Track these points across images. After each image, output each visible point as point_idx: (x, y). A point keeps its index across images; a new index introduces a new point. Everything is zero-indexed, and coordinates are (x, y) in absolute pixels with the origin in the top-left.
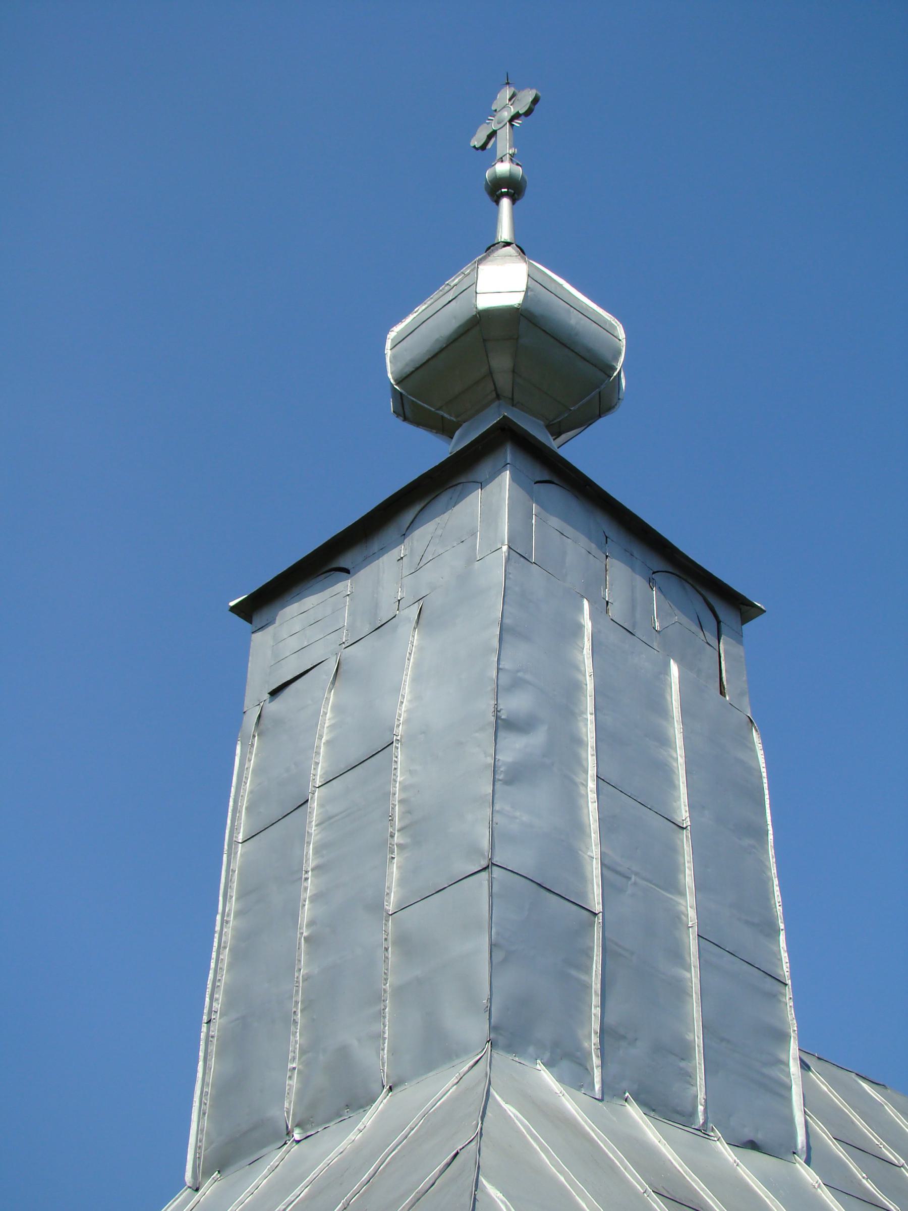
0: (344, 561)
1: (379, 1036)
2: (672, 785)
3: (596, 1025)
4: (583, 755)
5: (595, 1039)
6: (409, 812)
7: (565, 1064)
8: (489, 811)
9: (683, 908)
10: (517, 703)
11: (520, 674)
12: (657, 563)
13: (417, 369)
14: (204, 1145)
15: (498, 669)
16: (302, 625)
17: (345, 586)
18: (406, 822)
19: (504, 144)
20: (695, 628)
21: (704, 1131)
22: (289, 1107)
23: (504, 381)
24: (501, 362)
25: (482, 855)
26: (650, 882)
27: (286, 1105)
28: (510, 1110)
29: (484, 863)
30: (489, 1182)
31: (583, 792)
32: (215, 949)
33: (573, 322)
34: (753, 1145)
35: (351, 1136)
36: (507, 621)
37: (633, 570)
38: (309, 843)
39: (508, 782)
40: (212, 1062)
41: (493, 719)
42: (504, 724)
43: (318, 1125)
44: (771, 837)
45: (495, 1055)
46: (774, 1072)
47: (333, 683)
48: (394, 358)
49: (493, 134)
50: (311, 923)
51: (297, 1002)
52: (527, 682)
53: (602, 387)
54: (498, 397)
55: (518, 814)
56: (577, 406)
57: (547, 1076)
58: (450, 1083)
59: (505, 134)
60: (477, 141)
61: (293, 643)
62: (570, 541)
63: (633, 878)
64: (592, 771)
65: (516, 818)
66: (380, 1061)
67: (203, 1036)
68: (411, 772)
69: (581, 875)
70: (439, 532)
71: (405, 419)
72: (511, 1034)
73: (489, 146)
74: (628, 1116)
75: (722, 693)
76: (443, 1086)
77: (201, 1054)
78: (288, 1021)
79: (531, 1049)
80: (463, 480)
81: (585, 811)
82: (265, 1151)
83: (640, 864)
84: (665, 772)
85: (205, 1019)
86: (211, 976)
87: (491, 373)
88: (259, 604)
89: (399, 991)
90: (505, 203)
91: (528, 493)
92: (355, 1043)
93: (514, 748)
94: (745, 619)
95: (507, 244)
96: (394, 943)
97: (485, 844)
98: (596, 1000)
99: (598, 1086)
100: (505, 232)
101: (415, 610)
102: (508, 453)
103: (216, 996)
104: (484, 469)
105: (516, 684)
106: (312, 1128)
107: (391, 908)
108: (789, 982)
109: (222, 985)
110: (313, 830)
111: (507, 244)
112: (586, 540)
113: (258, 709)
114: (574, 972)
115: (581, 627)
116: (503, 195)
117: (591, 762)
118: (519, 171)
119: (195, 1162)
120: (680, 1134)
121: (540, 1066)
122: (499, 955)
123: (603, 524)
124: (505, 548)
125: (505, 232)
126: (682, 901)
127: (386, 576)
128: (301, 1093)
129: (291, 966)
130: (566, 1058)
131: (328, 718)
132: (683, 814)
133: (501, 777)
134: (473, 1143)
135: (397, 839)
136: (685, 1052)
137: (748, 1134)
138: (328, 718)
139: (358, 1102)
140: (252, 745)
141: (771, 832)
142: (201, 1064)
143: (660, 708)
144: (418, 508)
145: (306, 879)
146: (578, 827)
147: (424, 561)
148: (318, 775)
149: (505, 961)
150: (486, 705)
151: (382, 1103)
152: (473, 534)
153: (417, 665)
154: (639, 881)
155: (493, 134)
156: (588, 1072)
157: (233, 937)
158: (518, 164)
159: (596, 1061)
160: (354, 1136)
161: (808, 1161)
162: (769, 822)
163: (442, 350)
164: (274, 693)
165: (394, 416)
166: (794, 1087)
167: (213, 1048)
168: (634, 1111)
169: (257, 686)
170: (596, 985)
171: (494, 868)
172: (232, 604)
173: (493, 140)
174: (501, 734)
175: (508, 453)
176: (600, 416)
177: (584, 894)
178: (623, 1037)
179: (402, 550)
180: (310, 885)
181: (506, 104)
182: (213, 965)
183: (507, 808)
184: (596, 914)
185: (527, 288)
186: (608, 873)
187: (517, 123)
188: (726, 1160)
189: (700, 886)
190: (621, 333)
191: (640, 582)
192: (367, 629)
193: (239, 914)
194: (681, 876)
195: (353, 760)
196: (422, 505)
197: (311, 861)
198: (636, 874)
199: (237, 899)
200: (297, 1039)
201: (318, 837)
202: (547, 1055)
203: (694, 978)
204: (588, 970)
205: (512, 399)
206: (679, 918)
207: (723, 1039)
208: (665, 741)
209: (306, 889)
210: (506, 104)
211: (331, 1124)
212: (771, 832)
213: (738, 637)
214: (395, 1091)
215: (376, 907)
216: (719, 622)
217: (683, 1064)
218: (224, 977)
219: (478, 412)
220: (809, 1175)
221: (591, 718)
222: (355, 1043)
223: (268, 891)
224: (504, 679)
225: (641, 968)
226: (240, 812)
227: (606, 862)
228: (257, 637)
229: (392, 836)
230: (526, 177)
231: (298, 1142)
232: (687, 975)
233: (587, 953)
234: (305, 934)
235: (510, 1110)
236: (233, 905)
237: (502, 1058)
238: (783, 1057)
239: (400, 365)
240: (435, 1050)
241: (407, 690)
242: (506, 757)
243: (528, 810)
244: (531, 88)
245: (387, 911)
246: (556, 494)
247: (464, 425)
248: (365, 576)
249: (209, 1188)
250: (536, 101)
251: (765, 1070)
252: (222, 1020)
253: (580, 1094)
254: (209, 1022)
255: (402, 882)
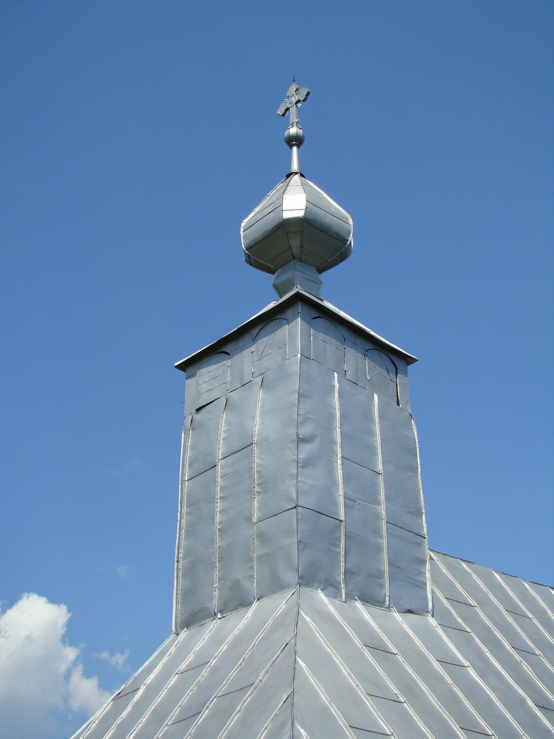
0: (227, 349)
1: (252, 576)
2: (375, 454)
3: (342, 570)
4: (336, 448)
5: (342, 576)
6: (261, 477)
7: (330, 589)
8: (295, 481)
9: (380, 511)
10: (306, 430)
11: (307, 416)
12: (368, 346)
13: (256, 244)
14: (179, 615)
15: (298, 415)
16: (210, 379)
17: (228, 362)
18: (260, 481)
19: (293, 115)
20: (386, 373)
21: (389, 607)
22: (215, 604)
23: (296, 251)
24: (295, 243)
25: (293, 501)
26: (365, 501)
27: (214, 603)
28: (308, 619)
29: (294, 505)
30: (300, 659)
31: (336, 465)
32: (178, 528)
33: (328, 221)
34: (410, 611)
35: (243, 622)
36: (301, 391)
37: (357, 351)
38: (218, 486)
39: (303, 467)
40: (180, 580)
41: (296, 438)
42: (301, 440)
43: (228, 612)
44: (419, 470)
45: (301, 590)
46: (420, 578)
47: (225, 409)
48: (245, 237)
49: (287, 109)
50: (220, 523)
51: (216, 558)
52: (311, 419)
53: (343, 249)
54: (294, 258)
55: (308, 481)
56: (331, 260)
57: (321, 595)
58: (283, 604)
59: (293, 110)
60: (280, 111)
61: (205, 387)
62: (327, 343)
63: (358, 501)
64: (339, 455)
65: (306, 483)
66: (253, 587)
67: (175, 567)
68: (262, 459)
69: (335, 504)
70: (270, 342)
71: (251, 265)
72: (307, 580)
73: (286, 115)
74: (357, 608)
75: (398, 404)
76: (280, 603)
77: (175, 575)
78: (213, 565)
79: (316, 584)
80: (279, 317)
81: (337, 473)
82: (206, 621)
83: (361, 495)
84: (372, 449)
85: (176, 560)
86: (177, 540)
87: (290, 248)
88: (189, 366)
89: (260, 558)
90: (295, 149)
91: (308, 324)
92: (242, 579)
93: (306, 450)
94: (408, 364)
95: (297, 173)
96: (257, 536)
97: (294, 496)
98: (342, 559)
99: (343, 596)
100: (295, 167)
101: (259, 380)
102: (300, 307)
103: (180, 551)
104: (289, 313)
105: (306, 420)
106: (225, 613)
107: (255, 520)
108: (426, 537)
109: (182, 545)
110: (219, 479)
111: (297, 173)
112: (336, 341)
113: (191, 416)
114: (333, 548)
115: (334, 386)
116: (293, 145)
117: (339, 450)
118: (300, 132)
119: (176, 622)
120: (378, 611)
121: (319, 591)
122: (301, 546)
123: (343, 331)
124: (299, 355)
125: (295, 167)
126: (379, 508)
127: (247, 360)
128: (220, 597)
129: (213, 542)
130: (330, 586)
131: (223, 427)
132: (380, 467)
133: (300, 465)
134: (293, 640)
135: (256, 489)
136: (381, 575)
137: (408, 607)
138: (223, 427)
139: (245, 604)
140: (189, 434)
141: (419, 468)
142: (175, 579)
143: (369, 418)
144: (259, 327)
145: (217, 502)
146: (335, 483)
147: (263, 355)
148: (220, 454)
149: (304, 548)
150: (292, 431)
151: (255, 605)
152: (285, 345)
153: (262, 407)
154: (362, 502)
155: (287, 109)
156: (339, 590)
157: (186, 524)
158: (300, 128)
159: (343, 585)
160: (244, 621)
161: (432, 616)
162: (419, 463)
163: (267, 236)
164: (198, 410)
165: (245, 263)
166: (428, 583)
167: (180, 574)
168: (359, 604)
169: (190, 407)
170: (342, 552)
171: (299, 507)
172: (176, 364)
173: (288, 112)
174: (300, 445)
175: (300, 307)
176: (342, 261)
177: (337, 513)
178: (354, 573)
179: (253, 348)
180: (219, 505)
181: (294, 95)
182: (178, 536)
183: (303, 479)
184: (342, 521)
185: (306, 207)
186: (348, 502)
187: (299, 105)
188: (397, 621)
189: (388, 499)
190: (351, 222)
191: (360, 356)
192: (238, 385)
193: (188, 514)
194: (379, 496)
195: (235, 448)
196: (262, 326)
197: (219, 495)
198: (359, 499)
199: (187, 507)
200: (217, 574)
201: (222, 483)
202: (322, 586)
203: (384, 542)
204: (339, 546)
205: (301, 259)
206: (378, 516)
207: (398, 567)
208: (372, 434)
209: (217, 507)
210: (294, 95)
211: (234, 612)
212: (419, 468)
213: (405, 373)
214: (260, 601)
215: (249, 519)
216: (396, 369)
217: (380, 581)
218: (183, 542)
219: (285, 264)
220: (433, 622)
221: (338, 430)
222: (242, 579)
223: (201, 503)
224: (301, 419)
225: (361, 543)
226: (186, 466)
227: (346, 496)
228: (189, 381)
229: (254, 488)
230: (304, 134)
231: (220, 619)
232: (382, 541)
233: (339, 539)
234: (218, 527)
235: (308, 619)
236: (185, 510)
237: (305, 590)
238: (423, 570)
239: (248, 241)
240: (276, 586)
241: (258, 419)
242: (302, 456)
243: (312, 479)
244: (306, 88)
245: (253, 522)
246: (321, 322)
247: (279, 270)
248: (237, 358)
249: (183, 634)
250: (308, 94)
251: (415, 578)
252: (184, 561)
253: (336, 601)
254: (178, 561)
255: (259, 509)
